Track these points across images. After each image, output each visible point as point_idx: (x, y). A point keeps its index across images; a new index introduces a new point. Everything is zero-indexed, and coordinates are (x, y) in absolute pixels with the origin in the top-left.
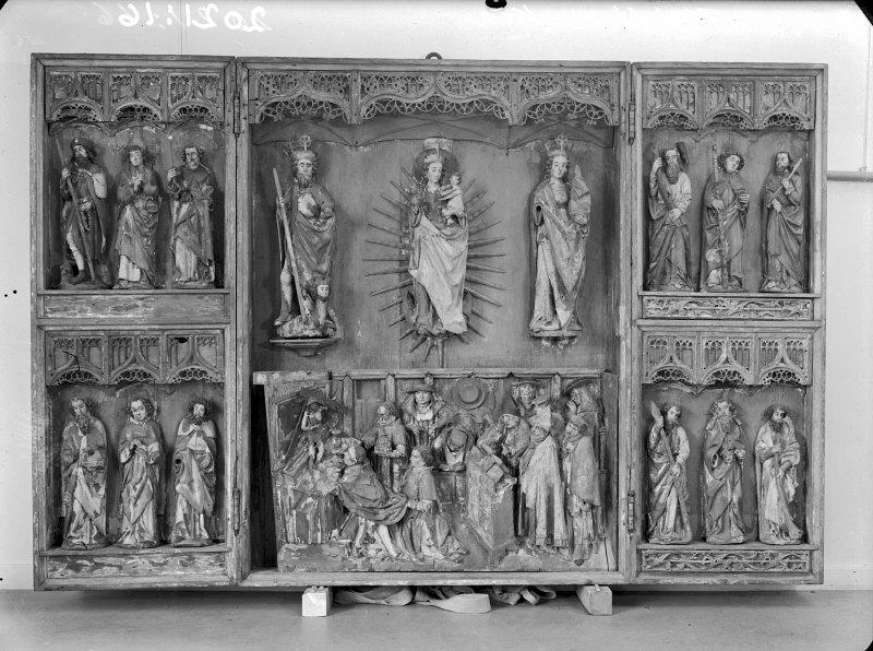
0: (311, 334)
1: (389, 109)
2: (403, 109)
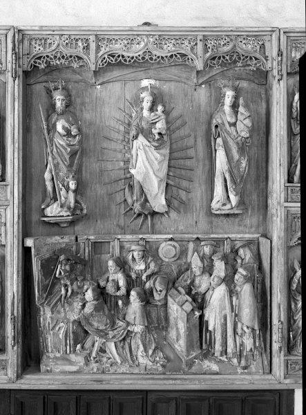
0: (65, 214)
1: (116, 60)
2: (125, 61)
